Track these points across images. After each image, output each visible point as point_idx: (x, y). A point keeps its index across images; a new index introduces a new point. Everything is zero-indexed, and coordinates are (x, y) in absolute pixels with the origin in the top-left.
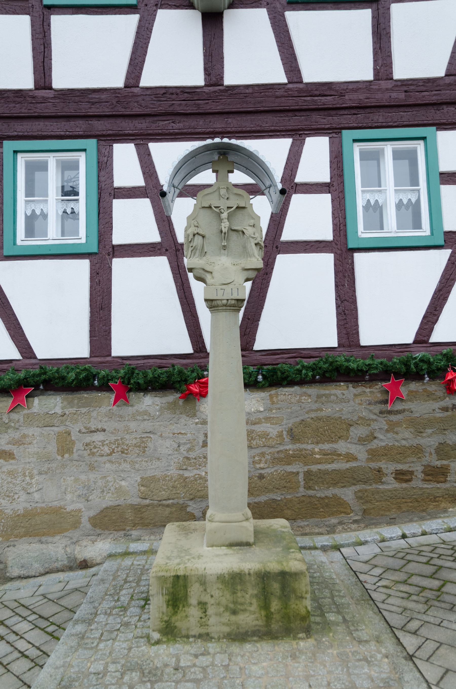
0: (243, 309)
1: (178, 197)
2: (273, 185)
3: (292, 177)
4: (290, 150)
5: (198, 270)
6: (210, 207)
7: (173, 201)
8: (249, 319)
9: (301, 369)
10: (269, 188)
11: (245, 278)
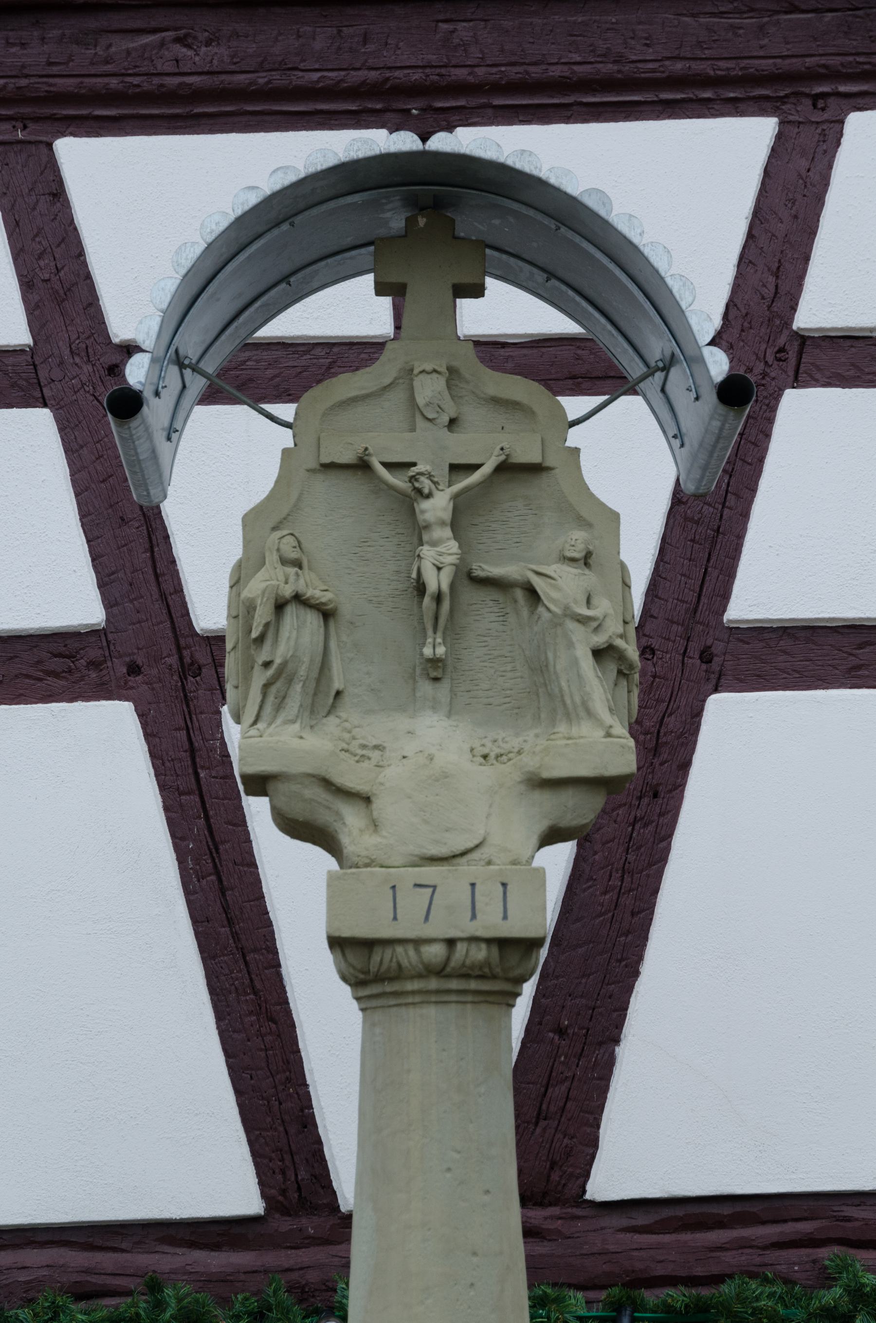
0: (529, 989)
2: (681, 355)
3: (777, 306)
4: (767, 172)
5: (294, 787)
6: (362, 466)
7: (172, 432)
8: (561, 1032)
9: (845, 1306)
10: (666, 369)
11: (541, 826)
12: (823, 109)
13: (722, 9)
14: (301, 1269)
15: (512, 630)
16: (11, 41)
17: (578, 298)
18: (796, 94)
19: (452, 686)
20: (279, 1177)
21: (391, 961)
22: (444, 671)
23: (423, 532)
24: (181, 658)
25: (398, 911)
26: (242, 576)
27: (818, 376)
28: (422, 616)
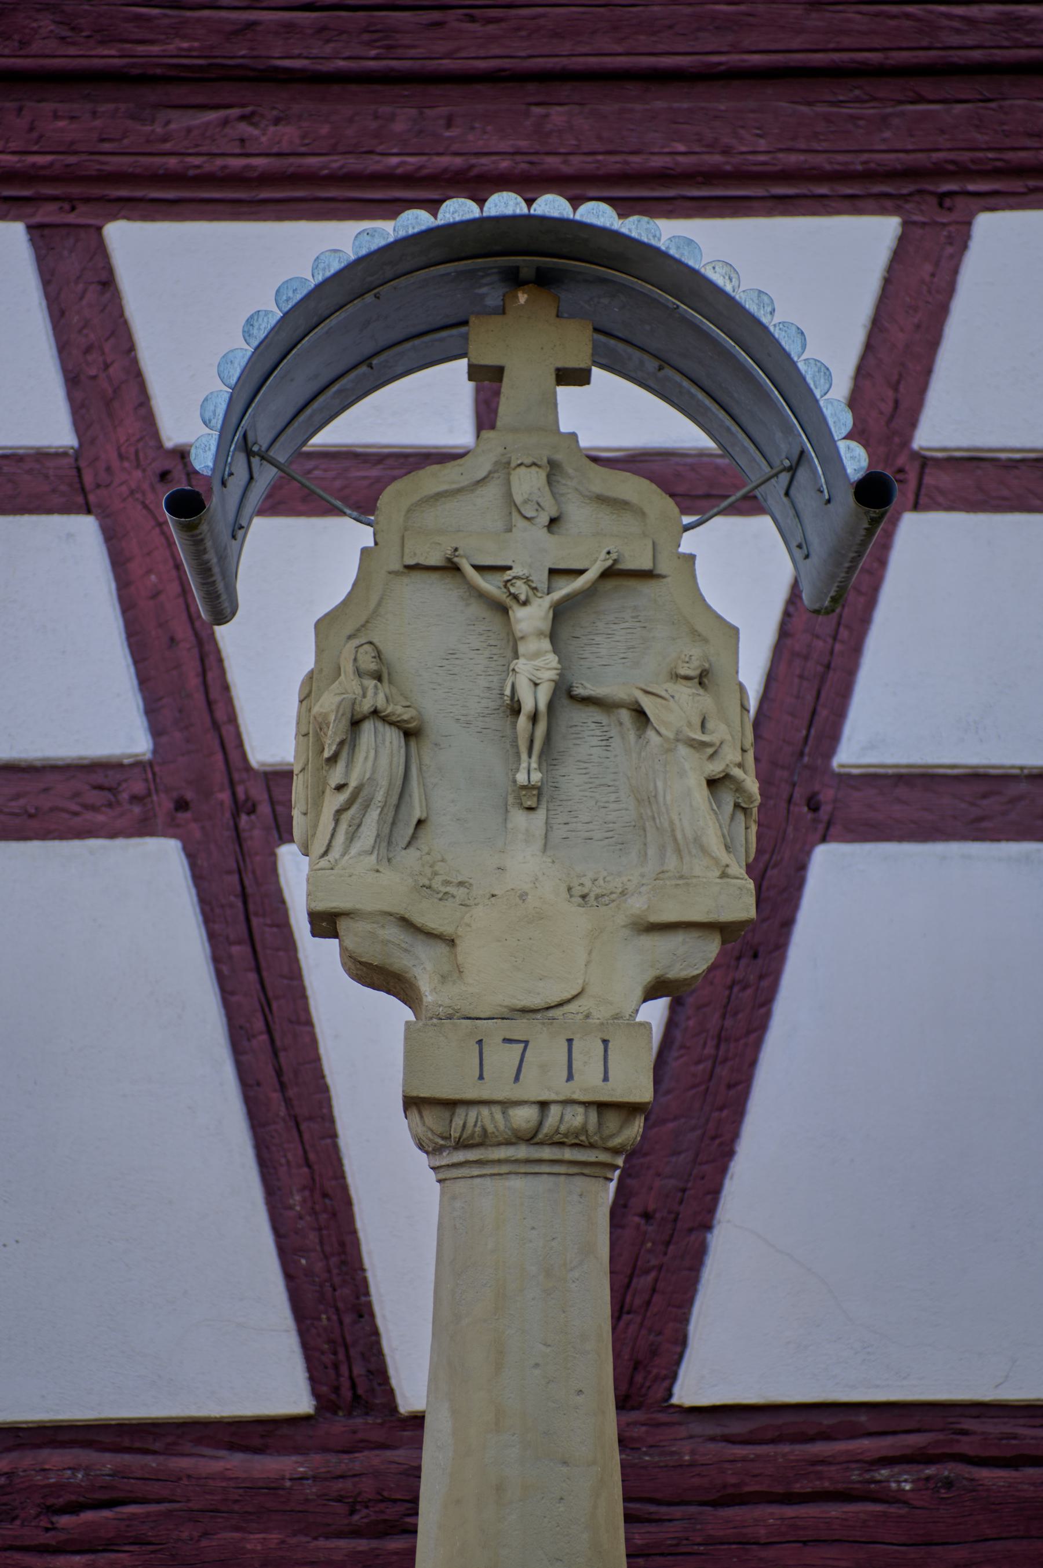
1: (261, 512)
7: (238, 530)
8: (647, 1216)
10: (793, 470)
11: (648, 977)
12: (950, 209)
13: (841, 98)
14: (355, 1476)
15: (616, 756)
16: (60, 114)
17: (694, 390)
18: (920, 192)
19: (547, 818)
20: (332, 1372)
21: (475, 1126)
22: (539, 800)
23: (519, 643)
24: (234, 794)
25: (485, 1068)
26: (314, 689)
27: (941, 499)
28: (516, 738)
